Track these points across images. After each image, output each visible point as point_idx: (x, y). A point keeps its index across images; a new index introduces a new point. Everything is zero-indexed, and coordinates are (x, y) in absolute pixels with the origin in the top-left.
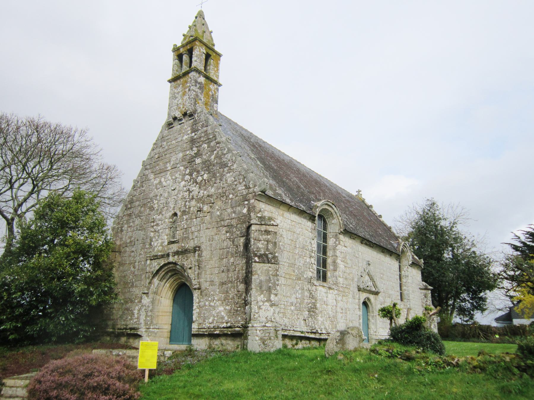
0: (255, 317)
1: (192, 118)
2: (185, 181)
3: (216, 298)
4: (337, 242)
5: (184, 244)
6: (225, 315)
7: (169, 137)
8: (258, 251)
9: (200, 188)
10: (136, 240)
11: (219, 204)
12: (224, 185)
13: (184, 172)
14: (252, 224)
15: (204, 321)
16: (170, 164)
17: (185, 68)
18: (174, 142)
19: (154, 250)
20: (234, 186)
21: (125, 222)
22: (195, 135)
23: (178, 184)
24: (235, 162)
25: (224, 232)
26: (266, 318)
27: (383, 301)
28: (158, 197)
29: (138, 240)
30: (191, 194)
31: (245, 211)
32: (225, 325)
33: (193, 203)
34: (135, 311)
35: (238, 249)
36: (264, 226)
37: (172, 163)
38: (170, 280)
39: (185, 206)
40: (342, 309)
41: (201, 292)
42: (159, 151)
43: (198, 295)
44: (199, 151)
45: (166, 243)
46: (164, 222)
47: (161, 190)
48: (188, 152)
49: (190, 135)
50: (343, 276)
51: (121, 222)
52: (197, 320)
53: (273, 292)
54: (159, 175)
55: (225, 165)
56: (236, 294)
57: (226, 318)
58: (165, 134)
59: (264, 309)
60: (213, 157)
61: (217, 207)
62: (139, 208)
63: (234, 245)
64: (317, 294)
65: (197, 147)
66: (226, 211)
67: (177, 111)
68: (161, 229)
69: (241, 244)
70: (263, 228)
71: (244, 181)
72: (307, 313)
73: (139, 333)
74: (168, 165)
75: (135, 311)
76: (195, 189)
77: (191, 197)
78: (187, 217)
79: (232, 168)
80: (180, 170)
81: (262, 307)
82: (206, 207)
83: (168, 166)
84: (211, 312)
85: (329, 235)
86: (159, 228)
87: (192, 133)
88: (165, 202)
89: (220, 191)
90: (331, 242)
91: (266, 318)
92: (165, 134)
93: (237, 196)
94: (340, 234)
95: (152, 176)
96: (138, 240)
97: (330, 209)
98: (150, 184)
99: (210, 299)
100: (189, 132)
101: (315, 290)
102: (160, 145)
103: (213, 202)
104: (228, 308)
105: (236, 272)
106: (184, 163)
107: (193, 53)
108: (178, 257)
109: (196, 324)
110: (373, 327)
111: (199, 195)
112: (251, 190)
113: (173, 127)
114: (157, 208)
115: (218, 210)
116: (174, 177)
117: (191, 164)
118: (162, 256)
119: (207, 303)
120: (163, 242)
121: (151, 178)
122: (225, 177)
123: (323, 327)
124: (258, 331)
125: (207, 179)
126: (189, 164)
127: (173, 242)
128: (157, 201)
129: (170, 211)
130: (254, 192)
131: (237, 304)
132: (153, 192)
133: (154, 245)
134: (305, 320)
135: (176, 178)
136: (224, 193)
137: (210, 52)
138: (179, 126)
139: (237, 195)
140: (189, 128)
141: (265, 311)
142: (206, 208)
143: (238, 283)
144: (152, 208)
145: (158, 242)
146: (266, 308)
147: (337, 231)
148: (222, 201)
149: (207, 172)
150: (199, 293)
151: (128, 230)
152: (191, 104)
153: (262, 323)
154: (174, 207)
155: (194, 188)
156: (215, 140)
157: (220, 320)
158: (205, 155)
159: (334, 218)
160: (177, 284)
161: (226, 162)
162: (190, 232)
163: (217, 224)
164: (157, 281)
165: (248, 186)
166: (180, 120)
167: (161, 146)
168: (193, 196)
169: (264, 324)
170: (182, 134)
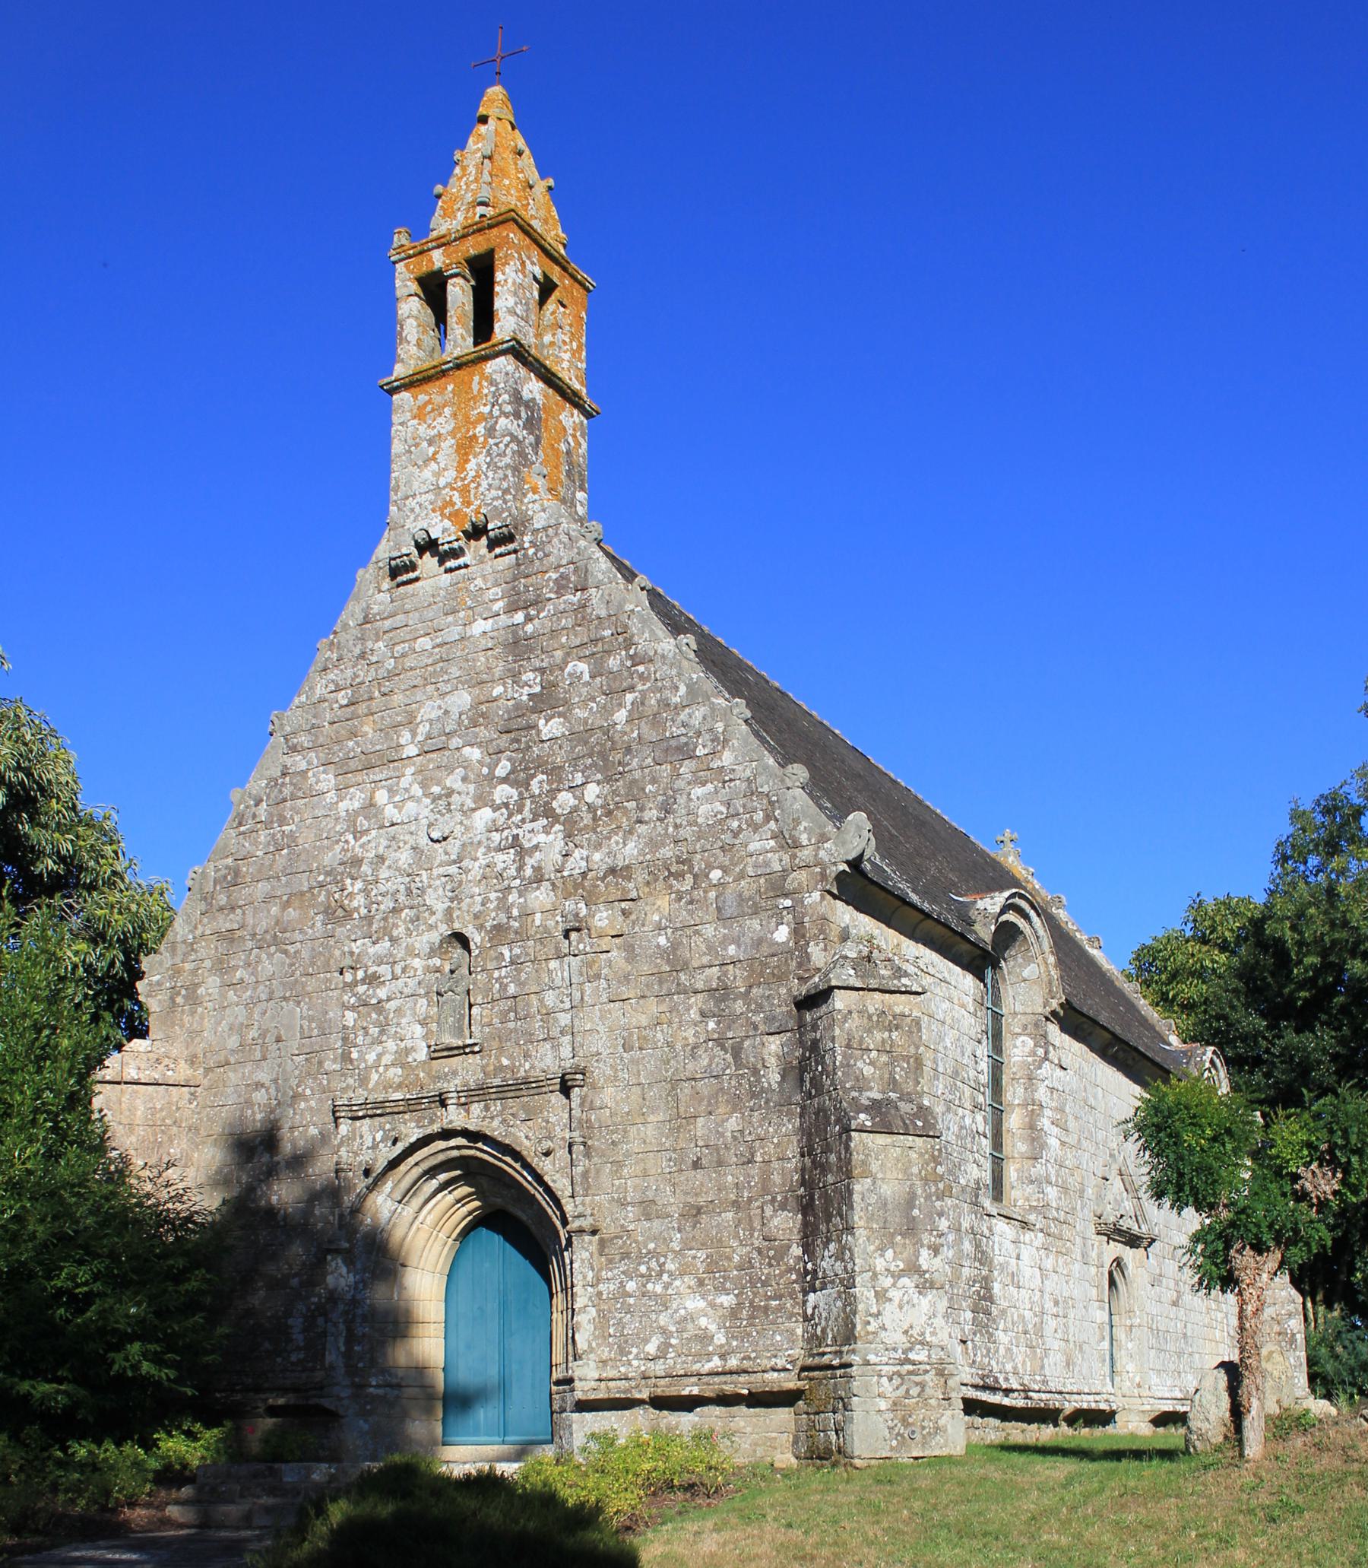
0: (870, 1328)
1: (511, 547)
2: (496, 808)
3: (670, 1266)
4: (1041, 1052)
5: (510, 1057)
6: (713, 1328)
7: (399, 620)
8: (861, 1090)
9: (568, 836)
10: (270, 1038)
11: (660, 907)
12: (682, 831)
13: (485, 770)
14: (831, 989)
15: (623, 1352)
16: (414, 734)
17: (460, 338)
18: (425, 643)
19: (363, 1081)
20: (726, 838)
21: (208, 964)
22: (529, 619)
23: (459, 817)
24: (726, 741)
25: (694, 1014)
26: (906, 1332)
27: (1158, 1271)
28: (365, 868)
29: (278, 1040)
30: (530, 862)
31: (782, 934)
32: (716, 1363)
33: (541, 897)
34: (290, 1321)
35: (758, 1081)
36: (877, 995)
37: (423, 730)
38: (440, 1196)
39: (504, 906)
40: (1056, 1303)
41: (602, 1243)
42: (356, 676)
43: (591, 1255)
44: (549, 687)
45: (422, 1054)
46: (404, 971)
47: (376, 841)
48: (498, 690)
49: (504, 621)
50: (1057, 1181)
51: (187, 966)
52: (591, 1350)
53: (926, 1238)
54: (359, 777)
55: (679, 749)
56: (759, 1251)
57: (720, 1339)
58: (376, 609)
59: (896, 1301)
60: (621, 716)
61: (656, 918)
62: (274, 910)
63: (738, 1067)
64: (993, 1247)
65: (542, 671)
66: (697, 932)
67: (436, 518)
68: (389, 999)
69: (772, 1062)
70: (875, 1002)
71: (768, 818)
72: (969, 1315)
73: (326, 1403)
74: (405, 737)
75: (290, 1321)
76: (549, 843)
77: (528, 872)
78: (517, 951)
79: (714, 765)
80: (466, 765)
81: (890, 1294)
82: (605, 914)
83: (402, 741)
84: (653, 1316)
85: (1011, 1025)
86: (382, 993)
87: (511, 610)
88: (402, 888)
89: (667, 852)
90: (1019, 1049)
91: (906, 1332)
92: (376, 609)
93: (742, 876)
94: (1047, 1019)
95: (327, 780)
96: (278, 1040)
97: (1021, 923)
98: (319, 812)
99: (643, 1269)
100: (499, 606)
101: (986, 1232)
102: (357, 651)
103: (633, 894)
104: (727, 1300)
105: (754, 1170)
106: (483, 733)
107: (499, 276)
108: (487, 1108)
109: (592, 1364)
110: (1130, 1367)
111: (569, 865)
112: (805, 854)
113: (417, 579)
114: (363, 911)
115: (659, 928)
116: (436, 789)
117: (518, 741)
118: (411, 1106)
119: (631, 1286)
120: (408, 1051)
121: (322, 787)
122: (682, 800)
123: (1009, 1367)
124: (884, 1380)
125: (600, 802)
126: (505, 737)
127: (452, 1051)
128: (359, 885)
129: (431, 927)
130: (819, 863)
131: (765, 1284)
132: (338, 848)
133: (362, 1059)
134: (964, 1342)
135: (450, 793)
136: (683, 863)
137: (556, 274)
138: (448, 575)
139: (742, 871)
140: (497, 591)
141: (901, 1307)
142: (603, 918)
143: (769, 1211)
144: (337, 913)
145: (379, 1049)
146: (906, 1298)
147: (1040, 1010)
148: (678, 891)
149: (599, 776)
150: (594, 1248)
151: (223, 996)
152: (506, 491)
153: (895, 1349)
154: (449, 911)
155: (542, 838)
156: (627, 649)
157: (696, 1347)
158: (584, 703)
159: (1030, 960)
160: (470, 1213)
161: (684, 739)
162: (534, 1010)
163: (660, 983)
164: (389, 1202)
165: (792, 837)
166: (456, 553)
167: (362, 656)
168: (537, 869)
169: (899, 1354)
170: (462, 614)
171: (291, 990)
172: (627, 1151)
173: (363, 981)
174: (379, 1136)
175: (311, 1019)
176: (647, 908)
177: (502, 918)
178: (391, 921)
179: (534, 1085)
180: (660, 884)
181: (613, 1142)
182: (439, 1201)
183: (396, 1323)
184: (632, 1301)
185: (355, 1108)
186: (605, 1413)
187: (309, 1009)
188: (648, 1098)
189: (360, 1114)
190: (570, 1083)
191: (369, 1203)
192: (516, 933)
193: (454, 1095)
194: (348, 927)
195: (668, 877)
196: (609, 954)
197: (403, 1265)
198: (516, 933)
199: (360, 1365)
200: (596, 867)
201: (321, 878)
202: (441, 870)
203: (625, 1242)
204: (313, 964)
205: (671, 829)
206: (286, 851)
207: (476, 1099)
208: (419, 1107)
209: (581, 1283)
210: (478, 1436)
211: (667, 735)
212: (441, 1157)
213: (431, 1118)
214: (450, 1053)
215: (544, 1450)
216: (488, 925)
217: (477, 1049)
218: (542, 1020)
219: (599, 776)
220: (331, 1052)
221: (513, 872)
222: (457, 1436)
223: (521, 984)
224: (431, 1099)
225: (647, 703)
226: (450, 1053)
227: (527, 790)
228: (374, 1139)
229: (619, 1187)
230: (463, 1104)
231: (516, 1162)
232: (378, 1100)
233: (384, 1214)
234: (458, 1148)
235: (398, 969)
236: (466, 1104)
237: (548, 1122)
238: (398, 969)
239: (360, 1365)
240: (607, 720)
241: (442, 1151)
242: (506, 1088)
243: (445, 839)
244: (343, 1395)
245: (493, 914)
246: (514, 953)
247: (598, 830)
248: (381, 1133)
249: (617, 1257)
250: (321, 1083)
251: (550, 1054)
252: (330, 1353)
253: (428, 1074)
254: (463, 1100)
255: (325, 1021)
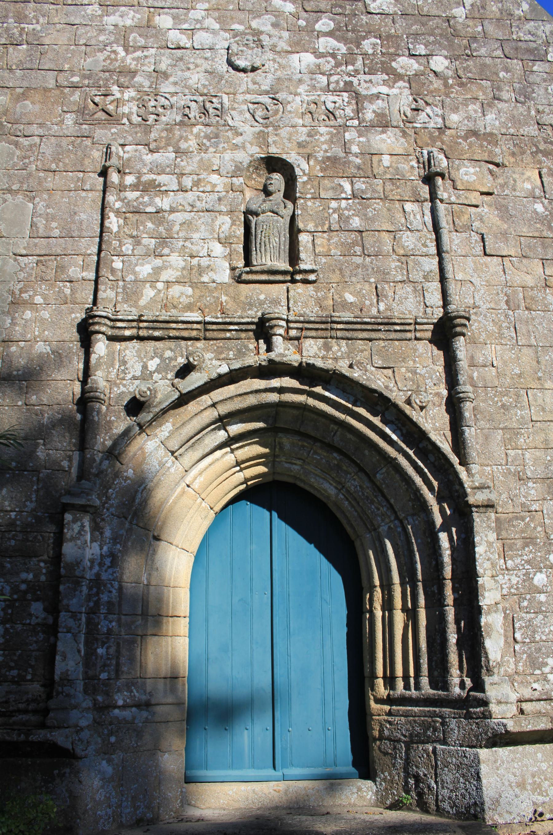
38: (218, 453)
68: (173, 210)
103: (498, 160)
145: (158, 262)
149: (446, 53)
160: (246, 481)
171: (22, 183)
172: (522, 417)
173: (135, 187)
174: (153, 364)
175: (49, 218)
176: (516, 176)
177: (338, 151)
178: (177, 133)
179: (398, 328)
180: (528, 158)
181: (503, 406)
182: (218, 460)
183: (145, 614)
184: (542, 598)
185: (119, 324)
186: (527, 747)
187: (48, 206)
188: (543, 362)
189: (127, 333)
190: (458, 329)
191: (133, 449)
192: (359, 168)
193: (283, 323)
194: (115, 130)
195: (536, 153)
196: (479, 210)
197: (157, 538)
198: (359, 168)
199: (104, 676)
200: (455, 126)
201: (76, 79)
202: (249, 97)
203: (527, 525)
204: (57, 160)
205: (533, 113)
206: (25, 46)
207: (313, 333)
208: (222, 335)
209: (489, 573)
210: (240, 768)
211: (515, 37)
212: (252, 400)
213: (239, 351)
214: (272, 278)
215: (359, 789)
216: (320, 155)
217: (312, 277)
218: (399, 260)
219: (446, 53)
220: (81, 258)
221: (349, 111)
222: (216, 769)
223: (365, 218)
224: (244, 327)
225: (487, 8)
226: (272, 278)
227: (358, 47)
228: (145, 367)
229: (515, 459)
230: (291, 339)
231: (375, 415)
232: (161, 318)
233: (153, 463)
234: (281, 390)
235: (188, 182)
236: (298, 339)
237: (415, 373)
238: (188, 182)
239: (104, 676)
240: (445, 12)
241: (257, 391)
242: (358, 327)
243: (254, 69)
244: (83, 723)
245: (325, 147)
246: (356, 187)
247: (452, 96)
248: (157, 361)
249: (519, 543)
250: (61, 291)
251: (411, 300)
252: (64, 658)
253: (234, 299)
254: (293, 333)
255: (73, 222)
